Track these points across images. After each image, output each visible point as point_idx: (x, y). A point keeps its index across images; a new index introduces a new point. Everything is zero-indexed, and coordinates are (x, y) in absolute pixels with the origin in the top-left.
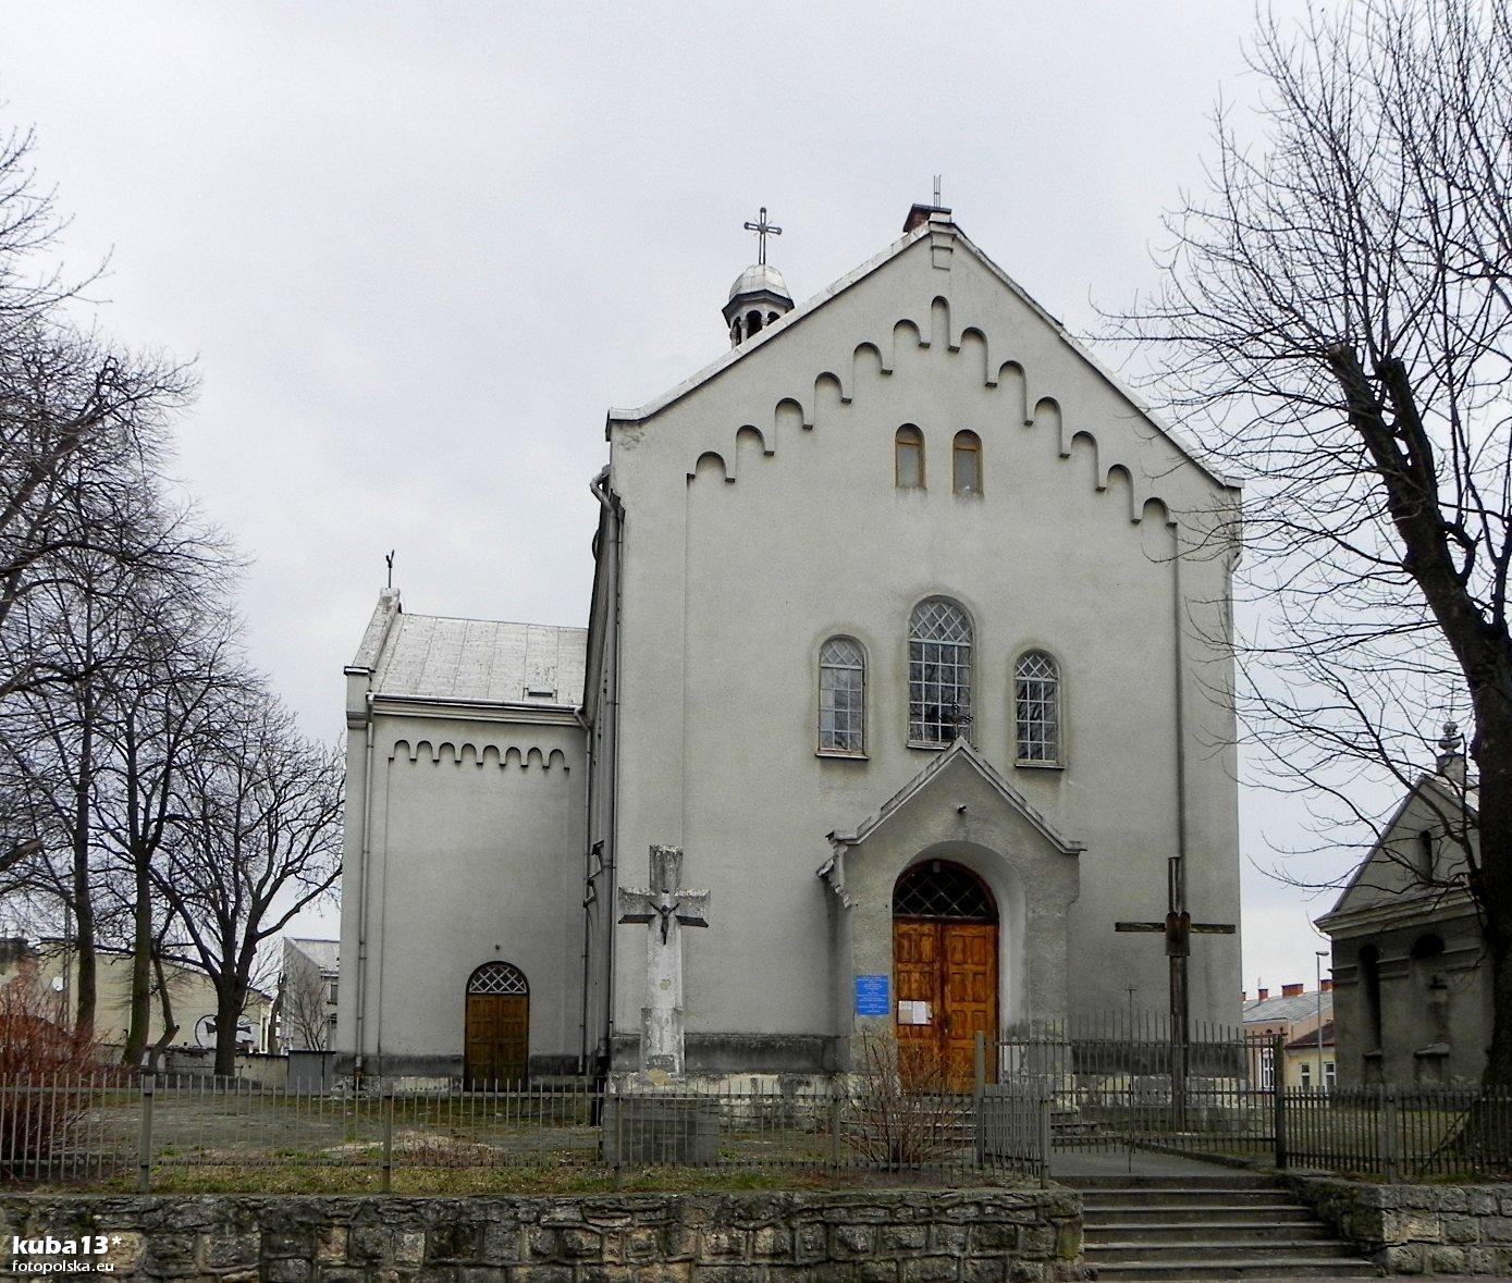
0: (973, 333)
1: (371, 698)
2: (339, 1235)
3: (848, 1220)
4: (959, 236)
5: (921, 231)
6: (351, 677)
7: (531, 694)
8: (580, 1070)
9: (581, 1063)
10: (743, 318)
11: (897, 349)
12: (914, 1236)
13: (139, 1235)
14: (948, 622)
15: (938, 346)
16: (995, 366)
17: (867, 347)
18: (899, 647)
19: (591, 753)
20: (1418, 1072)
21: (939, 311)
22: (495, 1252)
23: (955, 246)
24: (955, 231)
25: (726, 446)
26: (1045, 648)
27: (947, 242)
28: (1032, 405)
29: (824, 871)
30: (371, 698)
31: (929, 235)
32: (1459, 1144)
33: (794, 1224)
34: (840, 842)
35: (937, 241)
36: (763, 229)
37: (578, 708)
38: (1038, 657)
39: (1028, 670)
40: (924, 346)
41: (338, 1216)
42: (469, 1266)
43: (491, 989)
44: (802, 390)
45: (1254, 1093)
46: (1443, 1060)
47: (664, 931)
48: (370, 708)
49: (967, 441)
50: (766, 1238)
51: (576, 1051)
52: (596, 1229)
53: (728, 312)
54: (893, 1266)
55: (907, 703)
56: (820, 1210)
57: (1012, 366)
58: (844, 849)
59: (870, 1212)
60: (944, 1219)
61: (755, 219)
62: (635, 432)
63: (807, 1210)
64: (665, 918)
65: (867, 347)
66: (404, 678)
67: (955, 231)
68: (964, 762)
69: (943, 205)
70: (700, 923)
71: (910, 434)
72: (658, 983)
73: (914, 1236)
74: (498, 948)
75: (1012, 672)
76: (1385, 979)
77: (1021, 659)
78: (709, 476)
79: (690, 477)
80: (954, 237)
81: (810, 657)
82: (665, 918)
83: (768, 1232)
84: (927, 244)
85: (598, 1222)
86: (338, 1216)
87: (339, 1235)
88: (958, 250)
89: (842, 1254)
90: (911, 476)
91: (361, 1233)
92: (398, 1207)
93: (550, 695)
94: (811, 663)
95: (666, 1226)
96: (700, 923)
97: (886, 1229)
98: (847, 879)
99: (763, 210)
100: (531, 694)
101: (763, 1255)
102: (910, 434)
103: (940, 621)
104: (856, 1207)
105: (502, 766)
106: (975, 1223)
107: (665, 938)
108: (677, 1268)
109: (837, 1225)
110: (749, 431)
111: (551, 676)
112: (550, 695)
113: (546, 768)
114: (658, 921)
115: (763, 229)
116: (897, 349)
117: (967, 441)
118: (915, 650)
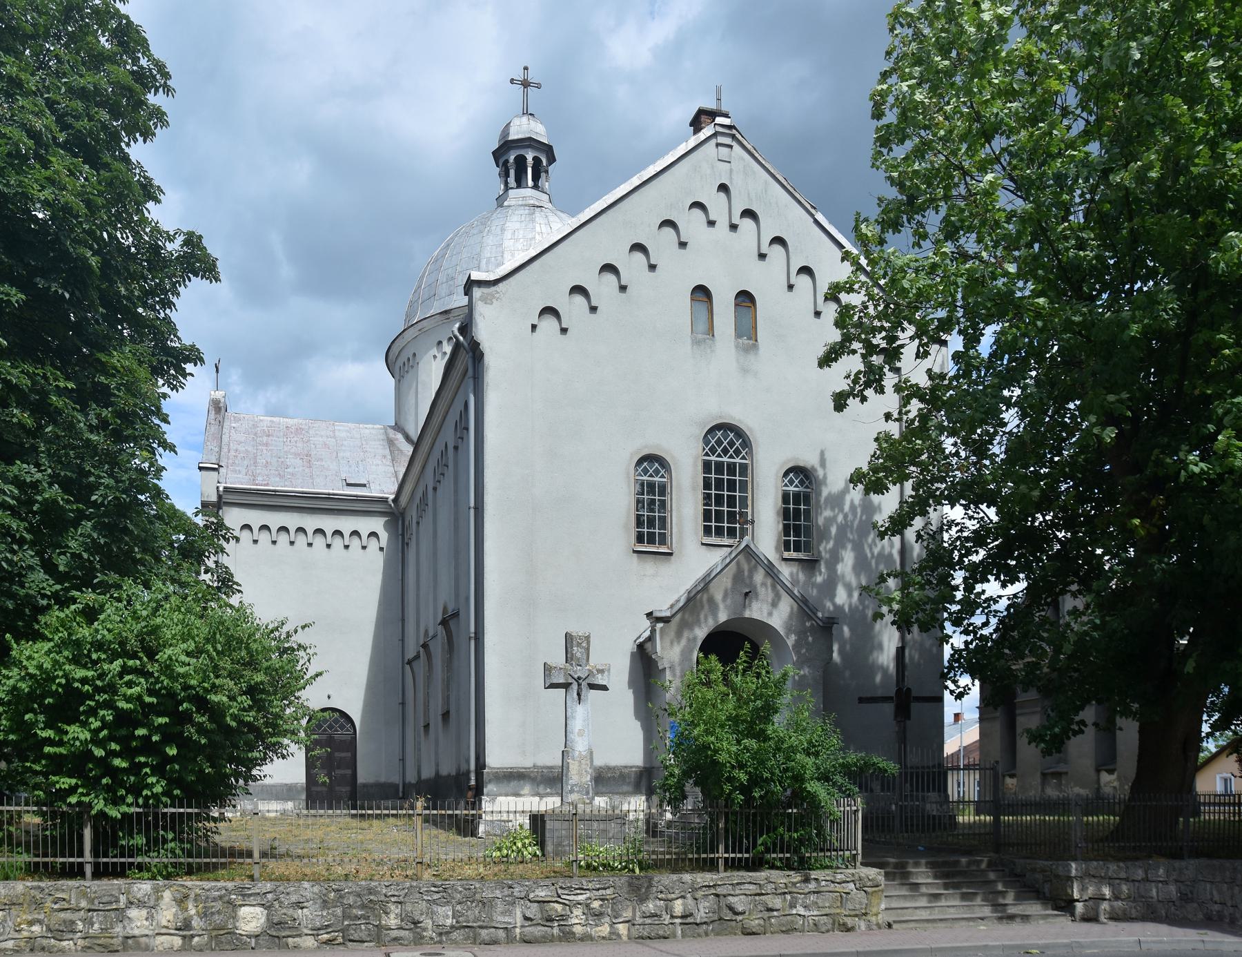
0: (749, 213)
1: (221, 489)
2: (394, 910)
3: (732, 893)
4: (738, 136)
5: (707, 131)
6: (203, 472)
7: (348, 485)
8: (401, 795)
9: (401, 789)
10: (512, 159)
11: (692, 224)
12: (777, 902)
13: (262, 909)
14: (731, 444)
15: (722, 224)
16: (766, 240)
17: (668, 223)
18: (695, 465)
19: (403, 535)
20: (1043, 784)
21: (722, 195)
22: (500, 918)
23: (734, 143)
24: (734, 132)
25: (562, 302)
26: (801, 464)
27: (728, 141)
28: (794, 270)
29: (641, 640)
30: (221, 489)
31: (715, 135)
32: (1116, 834)
33: (697, 896)
34: (659, 620)
35: (721, 140)
36: (526, 84)
37: (392, 497)
38: (800, 473)
39: (791, 482)
40: (711, 223)
41: (394, 896)
42: (481, 927)
43: (325, 730)
44: (620, 257)
45: (969, 802)
46: (1064, 776)
47: (579, 695)
48: (220, 497)
49: (745, 299)
50: (678, 907)
51: (396, 779)
52: (567, 902)
53: (497, 154)
54: (762, 922)
55: (701, 508)
56: (714, 886)
57: (778, 240)
58: (660, 625)
59: (747, 886)
60: (795, 890)
61: (519, 76)
62: (493, 289)
63: (706, 886)
64: (579, 685)
65: (668, 223)
66: (244, 471)
67: (734, 132)
68: (748, 552)
69: (724, 109)
70: (604, 688)
71: (702, 293)
72: (577, 731)
73: (777, 902)
74: (329, 697)
75: (780, 484)
76: (1021, 714)
77: (786, 474)
78: (549, 323)
79: (534, 327)
80: (733, 137)
81: (628, 474)
82: (579, 685)
83: (679, 902)
84: (713, 142)
85: (568, 897)
86: (394, 896)
87: (394, 910)
88: (736, 147)
89: (729, 916)
90: (702, 326)
91: (409, 908)
92: (433, 889)
93: (364, 485)
94: (629, 477)
95: (612, 899)
96: (604, 688)
97: (757, 898)
98: (662, 648)
99: (526, 68)
100: (348, 485)
101: (677, 917)
102: (702, 293)
103: (725, 443)
104: (738, 884)
105: (347, 547)
106: (814, 892)
107: (579, 699)
108: (620, 926)
109: (725, 896)
110: (578, 290)
111: (361, 468)
112: (364, 485)
113: (364, 548)
114: (575, 686)
115: (526, 84)
116: (692, 224)
117: (745, 299)
118: (707, 466)
